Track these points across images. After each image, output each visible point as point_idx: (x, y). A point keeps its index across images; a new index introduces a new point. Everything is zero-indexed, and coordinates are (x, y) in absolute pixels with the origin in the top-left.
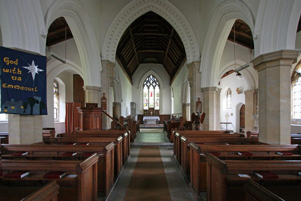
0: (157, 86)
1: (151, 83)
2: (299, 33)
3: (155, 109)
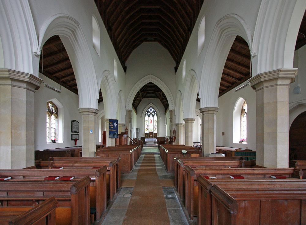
0: (155, 115)
1: (151, 113)
2: (219, 98)
3: (154, 133)
